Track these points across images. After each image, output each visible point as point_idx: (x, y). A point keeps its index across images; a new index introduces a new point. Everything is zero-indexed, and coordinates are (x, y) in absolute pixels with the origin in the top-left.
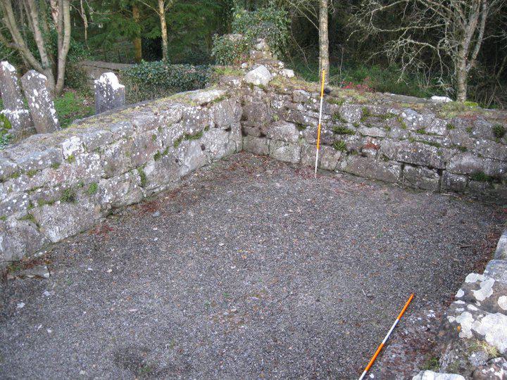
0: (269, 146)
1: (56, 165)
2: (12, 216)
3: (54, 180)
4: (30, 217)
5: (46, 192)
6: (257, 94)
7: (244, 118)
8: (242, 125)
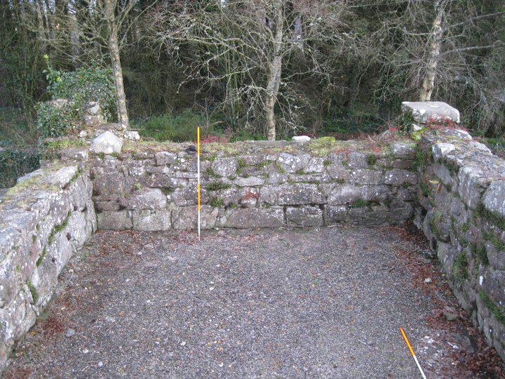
0: (132, 218)
6: (110, 164)
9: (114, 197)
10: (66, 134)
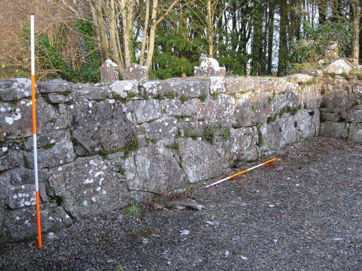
0: (348, 129)
1: (202, 98)
2: (161, 141)
3: (199, 113)
4: (175, 147)
5: (192, 123)
6: (338, 82)
7: (323, 106)
8: (321, 112)
9: (338, 110)
10: (308, 62)
